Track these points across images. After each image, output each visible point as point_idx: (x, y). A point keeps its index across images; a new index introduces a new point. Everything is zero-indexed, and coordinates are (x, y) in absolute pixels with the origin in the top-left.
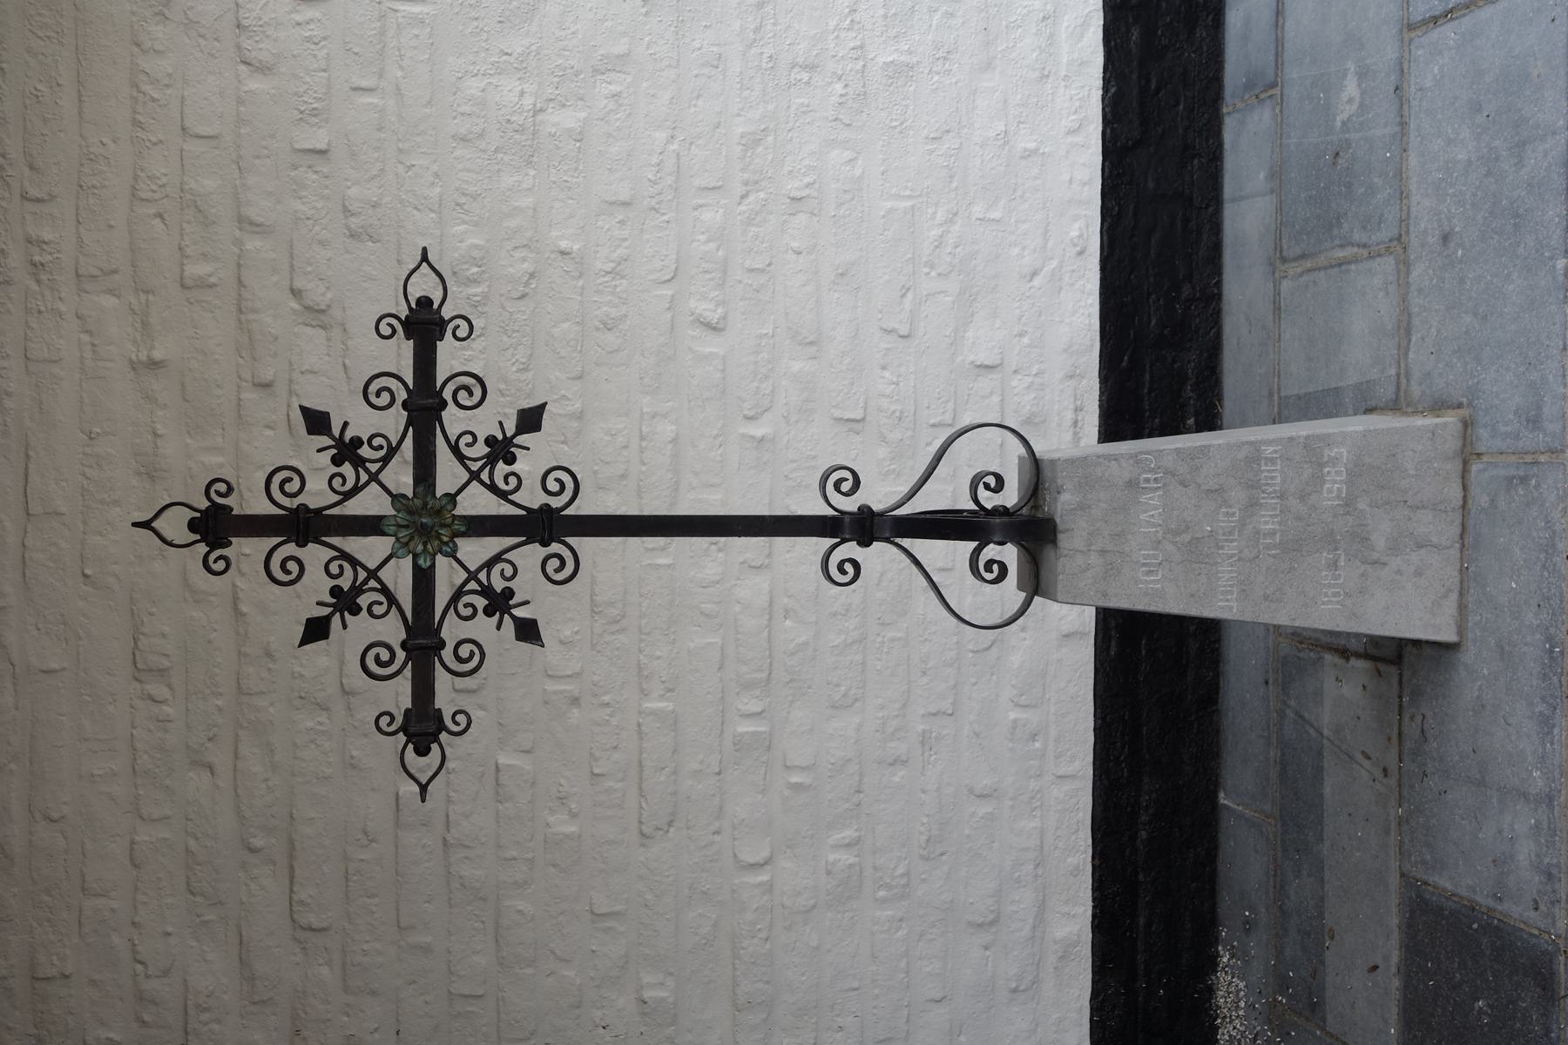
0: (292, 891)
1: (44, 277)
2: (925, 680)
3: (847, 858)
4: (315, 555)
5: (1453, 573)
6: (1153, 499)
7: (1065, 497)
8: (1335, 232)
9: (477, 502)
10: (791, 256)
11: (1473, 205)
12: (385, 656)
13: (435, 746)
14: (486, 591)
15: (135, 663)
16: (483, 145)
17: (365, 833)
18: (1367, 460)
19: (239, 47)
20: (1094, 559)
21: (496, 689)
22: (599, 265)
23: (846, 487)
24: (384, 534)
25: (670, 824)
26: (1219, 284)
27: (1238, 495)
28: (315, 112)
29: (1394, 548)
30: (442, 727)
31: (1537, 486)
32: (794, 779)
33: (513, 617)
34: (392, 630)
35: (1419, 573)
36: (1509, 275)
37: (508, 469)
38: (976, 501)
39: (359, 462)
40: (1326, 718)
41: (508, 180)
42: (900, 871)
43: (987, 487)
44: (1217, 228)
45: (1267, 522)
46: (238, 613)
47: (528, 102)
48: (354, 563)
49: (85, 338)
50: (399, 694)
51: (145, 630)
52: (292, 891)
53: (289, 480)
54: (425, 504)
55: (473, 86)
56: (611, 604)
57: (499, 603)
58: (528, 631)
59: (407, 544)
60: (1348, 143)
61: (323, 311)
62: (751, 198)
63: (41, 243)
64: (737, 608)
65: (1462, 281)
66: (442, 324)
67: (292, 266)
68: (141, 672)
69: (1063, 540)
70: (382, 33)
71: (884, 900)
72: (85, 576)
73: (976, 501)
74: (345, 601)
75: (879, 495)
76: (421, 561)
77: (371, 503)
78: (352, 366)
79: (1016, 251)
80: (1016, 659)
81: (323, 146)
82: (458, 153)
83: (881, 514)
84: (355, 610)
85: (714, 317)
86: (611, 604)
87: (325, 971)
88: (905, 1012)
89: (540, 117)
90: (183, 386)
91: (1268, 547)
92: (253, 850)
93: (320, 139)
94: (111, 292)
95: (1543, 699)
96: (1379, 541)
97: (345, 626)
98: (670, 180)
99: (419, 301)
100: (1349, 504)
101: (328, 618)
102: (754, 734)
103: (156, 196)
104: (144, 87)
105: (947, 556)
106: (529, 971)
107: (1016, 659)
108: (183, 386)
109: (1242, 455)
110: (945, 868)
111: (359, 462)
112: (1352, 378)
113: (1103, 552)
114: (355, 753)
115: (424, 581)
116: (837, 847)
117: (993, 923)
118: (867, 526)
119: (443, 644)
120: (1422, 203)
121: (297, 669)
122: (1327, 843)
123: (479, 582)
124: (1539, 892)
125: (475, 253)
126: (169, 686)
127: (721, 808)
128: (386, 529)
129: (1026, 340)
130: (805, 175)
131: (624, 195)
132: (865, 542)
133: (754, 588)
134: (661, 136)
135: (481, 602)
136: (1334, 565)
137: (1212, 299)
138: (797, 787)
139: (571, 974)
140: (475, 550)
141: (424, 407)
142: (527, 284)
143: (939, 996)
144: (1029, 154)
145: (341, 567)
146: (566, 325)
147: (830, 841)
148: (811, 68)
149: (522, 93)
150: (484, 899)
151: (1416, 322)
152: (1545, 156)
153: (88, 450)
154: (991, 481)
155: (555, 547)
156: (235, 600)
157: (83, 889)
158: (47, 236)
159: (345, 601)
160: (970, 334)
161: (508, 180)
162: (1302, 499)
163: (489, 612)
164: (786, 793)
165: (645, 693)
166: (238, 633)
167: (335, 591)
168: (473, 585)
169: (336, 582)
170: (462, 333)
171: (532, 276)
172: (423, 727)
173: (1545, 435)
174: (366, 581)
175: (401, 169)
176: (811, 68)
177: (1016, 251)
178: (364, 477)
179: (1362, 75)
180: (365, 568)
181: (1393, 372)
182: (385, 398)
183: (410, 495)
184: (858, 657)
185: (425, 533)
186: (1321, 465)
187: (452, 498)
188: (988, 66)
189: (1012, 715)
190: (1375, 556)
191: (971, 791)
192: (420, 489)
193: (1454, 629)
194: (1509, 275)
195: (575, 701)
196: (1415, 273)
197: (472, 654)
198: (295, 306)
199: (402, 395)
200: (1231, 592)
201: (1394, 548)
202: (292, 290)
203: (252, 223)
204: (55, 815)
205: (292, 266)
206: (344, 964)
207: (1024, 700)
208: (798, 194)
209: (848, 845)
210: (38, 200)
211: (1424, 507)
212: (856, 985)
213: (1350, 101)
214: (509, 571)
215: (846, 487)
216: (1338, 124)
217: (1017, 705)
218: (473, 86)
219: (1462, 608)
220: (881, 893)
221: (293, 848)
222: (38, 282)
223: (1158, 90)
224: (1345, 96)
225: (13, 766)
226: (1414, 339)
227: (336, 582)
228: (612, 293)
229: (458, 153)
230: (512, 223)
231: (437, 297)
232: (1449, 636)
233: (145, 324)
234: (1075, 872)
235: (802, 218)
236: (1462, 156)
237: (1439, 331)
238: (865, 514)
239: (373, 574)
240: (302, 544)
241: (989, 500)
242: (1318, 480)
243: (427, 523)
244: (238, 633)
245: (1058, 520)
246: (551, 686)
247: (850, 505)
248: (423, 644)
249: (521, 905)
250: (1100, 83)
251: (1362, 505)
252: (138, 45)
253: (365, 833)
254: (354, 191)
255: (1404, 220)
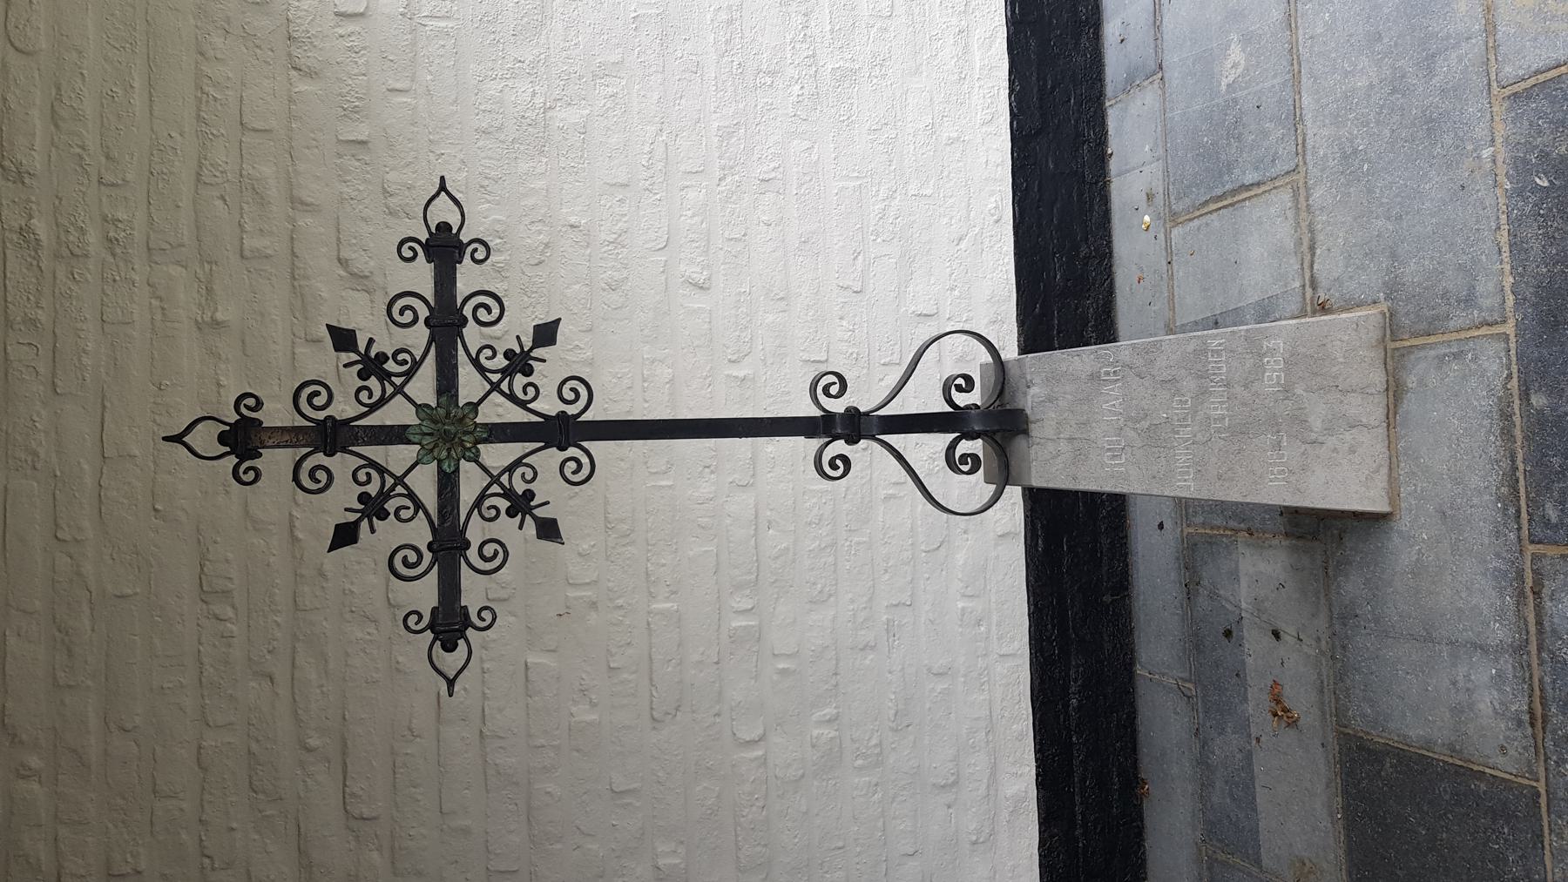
0: (345, 785)
1: (118, 251)
2: (887, 577)
3: (828, 732)
4: (341, 464)
5: (1381, 448)
6: (1113, 390)
7: (1034, 390)
8: (1226, 178)
9: (498, 411)
10: (763, 228)
11: (1378, 123)
12: (413, 557)
13: (461, 642)
14: (508, 493)
15: (201, 585)
16: (502, 137)
17: (410, 729)
18: (1302, 350)
19: (290, 55)
20: (1063, 446)
21: (512, 582)
22: (603, 236)
23: (834, 390)
24: (409, 442)
25: (677, 709)
26: (1109, 244)
27: (1189, 384)
28: (356, 110)
29: (1329, 430)
30: (467, 623)
31: (1475, 359)
32: (781, 666)
33: (534, 517)
34: (420, 533)
35: (1352, 451)
36: (1425, 174)
37: (526, 380)
38: (950, 402)
39: (385, 376)
40: (1244, 595)
41: (523, 166)
42: (874, 742)
43: (959, 389)
44: (1105, 200)
45: (1216, 408)
46: (294, 539)
47: (539, 100)
48: (382, 471)
49: (155, 302)
50: (425, 594)
51: (210, 557)
52: (345, 785)
53: (317, 394)
54: (448, 413)
55: (492, 88)
56: (622, 521)
57: (521, 505)
58: (549, 530)
59: (432, 450)
60: (1235, 101)
61: (366, 277)
62: (729, 179)
63: (116, 221)
64: (728, 521)
65: (1370, 191)
66: (460, 247)
67: (339, 239)
68: (206, 592)
69: (1035, 430)
70: (414, 44)
71: (861, 768)
72: (156, 510)
73: (950, 402)
74: (373, 507)
75: (864, 397)
76: (445, 467)
77: (397, 413)
78: (376, 288)
79: (946, 220)
80: (960, 558)
81: (363, 138)
82: (480, 143)
83: (867, 414)
84: (383, 515)
85: (700, 279)
86: (622, 521)
87: (375, 855)
88: (884, 866)
89: (549, 114)
90: (243, 342)
91: (1218, 431)
92: (309, 750)
93: (362, 131)
94: (178, 263)
95: (1498, 555)
96: (1317, 424)
97: (373, 531)
98: (660, 166)
99: (438, 226)
100: (1287, 390)
101: (356, 523)
102: (745, 627)
103: (219, 181)
104: (206, 89)
105: (926, 449)
106: (559, 846)
107: (960, 558)
108: (243, 342)
109: (1190, 348)
110: (911, 738)
111: (385, 376)
112: (1253, 297)
113: (1071, 439)
114: (400, 659)
115: (448, 484)
116: (820, 723)
117: (955, 783)
118: (855, 426)
119: (467, 545)
120: (1318, 133)
121: (347, 586)
122: (1251, 704)
123: (501, 485)
124: (1506, 738)
125: (498, 227)
126: (233, 607)
127: (720, 693)
128: (411, 437)
129: (956, 293)
130: (771, 160)
131: (622, 179)
132: (852, 441)
133: (770, 449)
134: (652, 129)
135: (503, 504)
136: (1278, 446)
137: (1104, 255)
138: (784, 672)
139: (595, 847)
140: (497, 455)
141: (446, 322)
142: (542, 253)
143: (911, 851)
144: (952, 142)
145: (368, 474)
146: (577, 287)
147: (814, 718)
148: (772, 73)
149: (534, 94)
150: (517, 784)
151: (1320, 237)
152: (1460, 60)
153: (159, 400)
154: (960, 381)
155: (572, 451)
156: (292, 527)
157: (154, 792)
158: (120, 215)
159: (373, 507)
160: (910, 289)
161: (523, 166)
162: (1246, 386)
163: (511, 513)
164: (775, 677)
165: (652, 596)
166: (294, 557)
167: (363, 498)
168: (496, 489)
169: (363, 489)
170: (480, 255)
171: (547, 245)
172: (450, 624)
173: (1481, 310)
174: (393, 488)
175: (432, 157)
176: (772, 73)
177: (946, 220)
178: (389, 390)
179: (1246, 40)
180: (392, 475)
181: (1297, 284)
182: (408, 316)
183: (434, 405)
184: (831, 559)
185: (448, 439)
186: (1261, 356)
187: (474, 407)
188: (917, 71)
189: (960, 605)
190: (1313, 436)
191: (929, 670)
192: (444, 399)
193: (1386, 500)
194: (1425, 174)
195: (593, 605)
196: (1317, 194)
197: (496, 553)
198: (343, 273)
199: (423, 312)
200: (1188, 473)
201: (1329, 430)
202: (339, 260)
203: (302, 203)
204: (129, 726)
205: (339, 239)
206: (392, 849)
207: (969, 591)
208: (766, 177)
209: (829, 721)
210: (113, 185)
211: (1354, 391)
212: (840, 844)
213: (1235, 66)
214: (529, 475)
215: (834, 390)
216: (1224, 88)
217: (964, 596)
218: (492, 88)
219: (1392, 480)
220: (859, 762)
221: (345, 745)
222: (114, 255)
223: (1053, 88)
224: (1228, 64)
225: (89, 683)
226: (1318, 252)
227: (363, 489)
228: (616, 260)
229: (480, 143)
230: (530, 202)
231: (454, 219)
232: (1381, 507)
233: (209, 290)
234: (1020, 737)
235: (770, 197)
236: (1362, 83)
237: (1346, 239)
238: (853, 414)
239: (399, 480)
240: (330, 454)
241: (961, 399)
242: (1260, 368)
243: (450, 431)
244: (294, 557)
245: (1028, 411)
246: (572, 593)
247: (837, 406)
248: (449, 545)
249: (550, 787)
250: (1006, 84)
251: (1299, 391)
252: (202, 54)
253: (410, 729)
254: (392, 176)
255: (1301, 149)
